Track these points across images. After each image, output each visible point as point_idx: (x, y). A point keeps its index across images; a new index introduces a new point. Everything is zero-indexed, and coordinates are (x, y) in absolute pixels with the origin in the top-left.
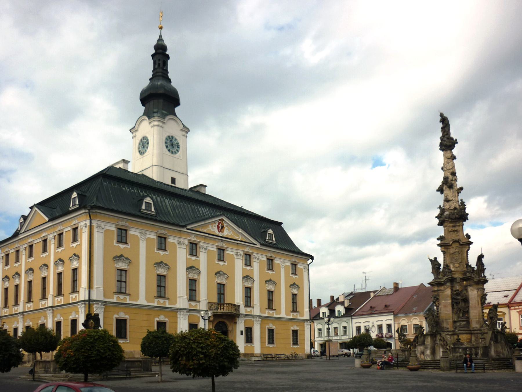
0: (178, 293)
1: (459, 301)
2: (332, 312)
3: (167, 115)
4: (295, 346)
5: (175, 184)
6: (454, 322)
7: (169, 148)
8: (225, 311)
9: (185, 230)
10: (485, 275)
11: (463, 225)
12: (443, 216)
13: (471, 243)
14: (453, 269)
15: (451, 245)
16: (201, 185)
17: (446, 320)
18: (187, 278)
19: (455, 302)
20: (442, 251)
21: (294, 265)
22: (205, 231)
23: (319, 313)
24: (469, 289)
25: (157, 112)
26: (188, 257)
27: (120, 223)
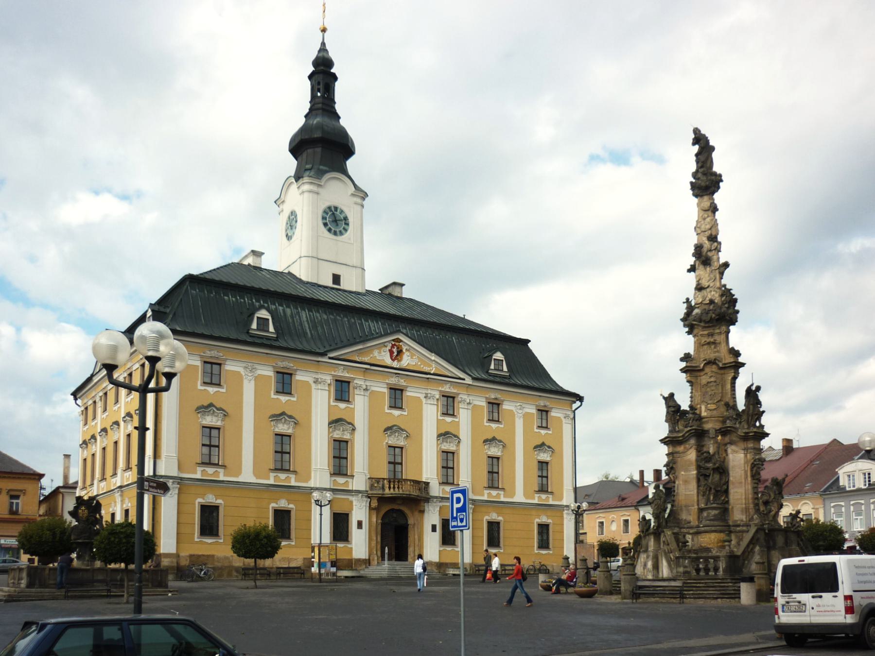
3: (326, 172)
4: (544, 552)
5: (339, 284)
6: (701, 510)
8: (401, 492)
9: (325, 359)
10: (763, 422)
11: (728, 332)
12: (691, 318)
13: (743, 365)
14: (704, 414)
15: (702, 370)
19: (702, 475)
20: (688, 381)
21: (544, 412)
22: (366, 359)
24: (730, 449)
25: (310, 169)
26: (440, 418)
27: (208, 353)
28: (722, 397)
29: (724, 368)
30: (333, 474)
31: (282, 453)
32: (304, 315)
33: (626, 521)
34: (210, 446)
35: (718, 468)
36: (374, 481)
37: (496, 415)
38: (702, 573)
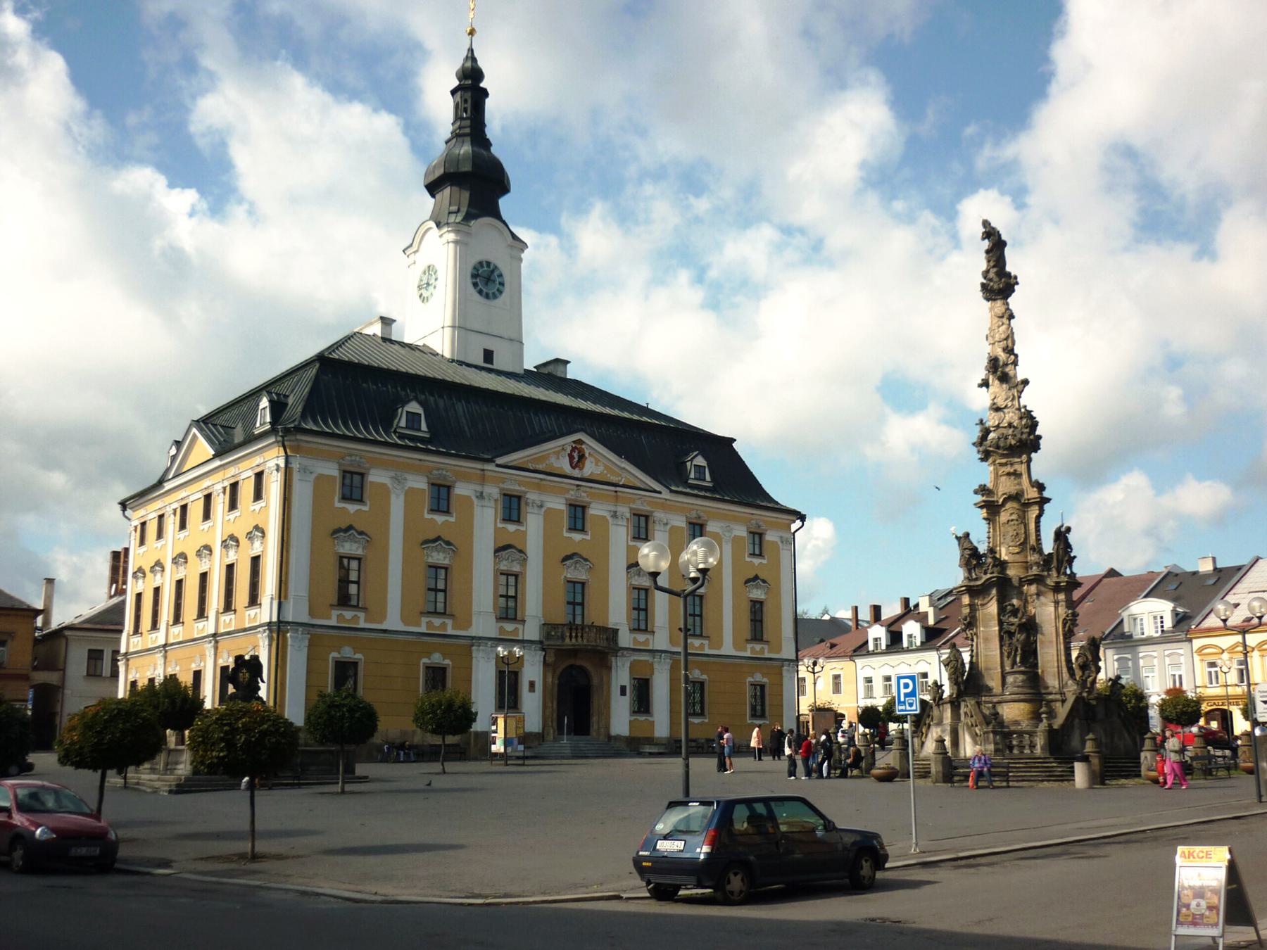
0: (474, 603)
2: (895, 639)
7: (480, 286)
9: (491, 467)
10: (1075, 570)
11: (1029, 461)
13: (1048, 500)
16: (557, 361)
19: (1005, 634)
21: (757, 536)
23: (867, 642)
30: (499, 619)
32: (460, 407)
33: (837, 677)
36: (549, 628)
38: (1016, 751)
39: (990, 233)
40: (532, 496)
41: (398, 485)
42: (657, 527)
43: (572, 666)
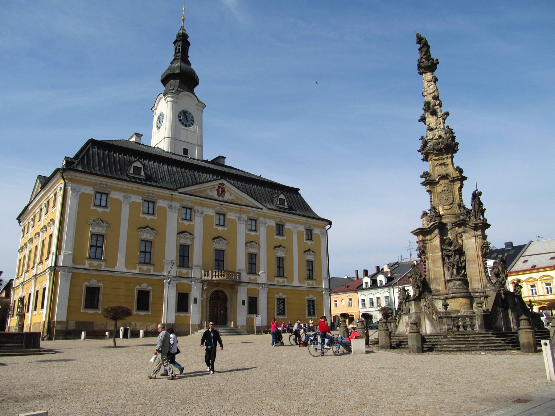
1: (451, 253)
2: (374, 282)
3: (182, 91)
9: (175, 193)
11: (452, 157)
12: (427, 148)
13: (465, 178)
16: (220, 157)
17: (436, 279)
18: (178, 243)
20: (428, 191)
23: (362, 284)
26: (248, 232)
28: (453, 201)
29: (453, 181)
31: (184, 256)
34: (96, 247)
35: (458, 250)
37: (281, 232)
38: (461, 329)
39: (420, 40)
40: (197, 208)
41: (126, 199)
42: (261, 225)
43: (217, 291)
